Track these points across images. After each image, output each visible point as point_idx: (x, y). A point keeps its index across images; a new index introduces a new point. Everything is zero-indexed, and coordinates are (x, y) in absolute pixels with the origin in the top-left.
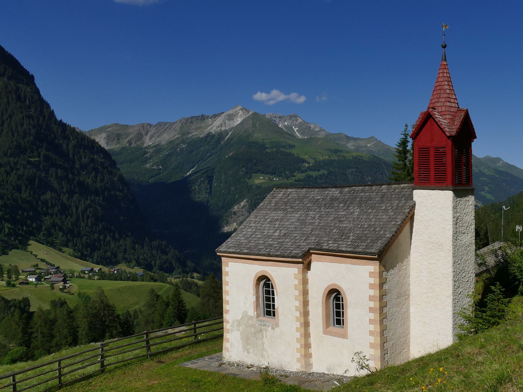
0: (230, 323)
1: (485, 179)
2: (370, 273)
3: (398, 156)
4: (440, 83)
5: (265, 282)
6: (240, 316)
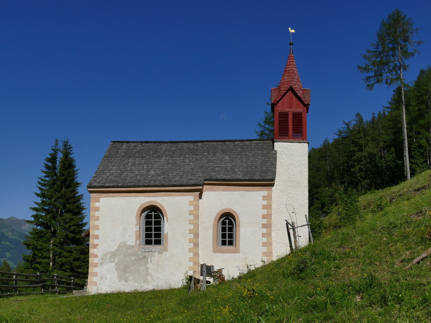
0: (100, 257)
1: (7, 243)
2: (263, 196)
3: (45, 172)
4: (292, 69)
5: (148, 212)
6: (116, 248)
